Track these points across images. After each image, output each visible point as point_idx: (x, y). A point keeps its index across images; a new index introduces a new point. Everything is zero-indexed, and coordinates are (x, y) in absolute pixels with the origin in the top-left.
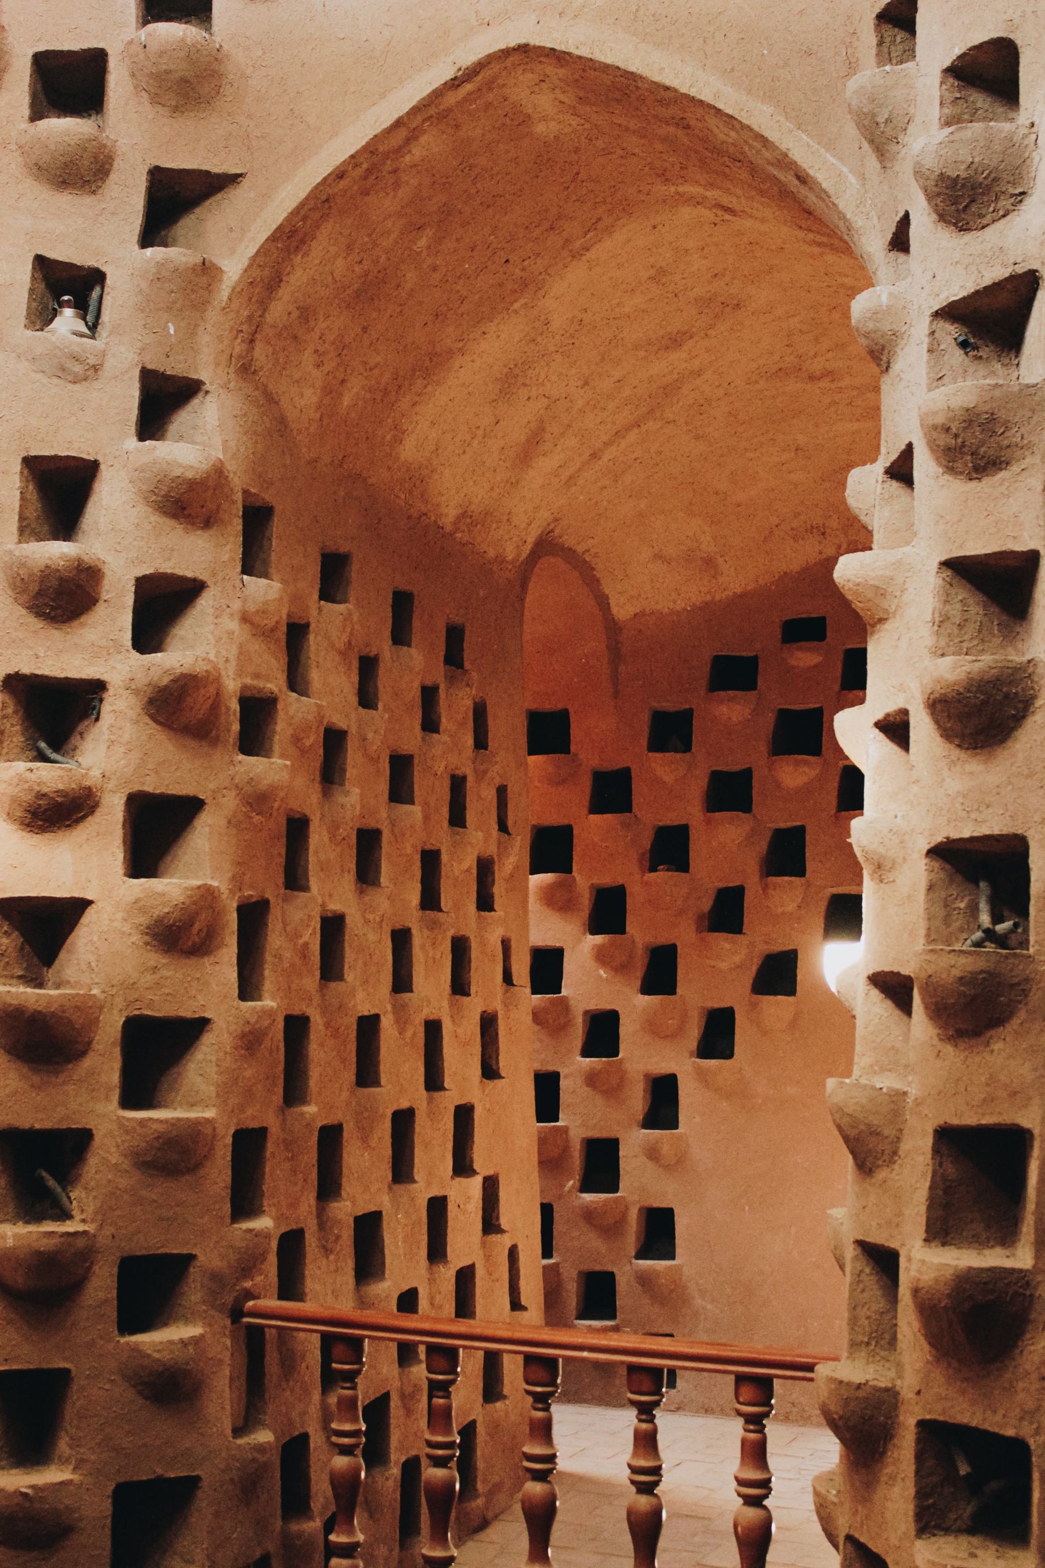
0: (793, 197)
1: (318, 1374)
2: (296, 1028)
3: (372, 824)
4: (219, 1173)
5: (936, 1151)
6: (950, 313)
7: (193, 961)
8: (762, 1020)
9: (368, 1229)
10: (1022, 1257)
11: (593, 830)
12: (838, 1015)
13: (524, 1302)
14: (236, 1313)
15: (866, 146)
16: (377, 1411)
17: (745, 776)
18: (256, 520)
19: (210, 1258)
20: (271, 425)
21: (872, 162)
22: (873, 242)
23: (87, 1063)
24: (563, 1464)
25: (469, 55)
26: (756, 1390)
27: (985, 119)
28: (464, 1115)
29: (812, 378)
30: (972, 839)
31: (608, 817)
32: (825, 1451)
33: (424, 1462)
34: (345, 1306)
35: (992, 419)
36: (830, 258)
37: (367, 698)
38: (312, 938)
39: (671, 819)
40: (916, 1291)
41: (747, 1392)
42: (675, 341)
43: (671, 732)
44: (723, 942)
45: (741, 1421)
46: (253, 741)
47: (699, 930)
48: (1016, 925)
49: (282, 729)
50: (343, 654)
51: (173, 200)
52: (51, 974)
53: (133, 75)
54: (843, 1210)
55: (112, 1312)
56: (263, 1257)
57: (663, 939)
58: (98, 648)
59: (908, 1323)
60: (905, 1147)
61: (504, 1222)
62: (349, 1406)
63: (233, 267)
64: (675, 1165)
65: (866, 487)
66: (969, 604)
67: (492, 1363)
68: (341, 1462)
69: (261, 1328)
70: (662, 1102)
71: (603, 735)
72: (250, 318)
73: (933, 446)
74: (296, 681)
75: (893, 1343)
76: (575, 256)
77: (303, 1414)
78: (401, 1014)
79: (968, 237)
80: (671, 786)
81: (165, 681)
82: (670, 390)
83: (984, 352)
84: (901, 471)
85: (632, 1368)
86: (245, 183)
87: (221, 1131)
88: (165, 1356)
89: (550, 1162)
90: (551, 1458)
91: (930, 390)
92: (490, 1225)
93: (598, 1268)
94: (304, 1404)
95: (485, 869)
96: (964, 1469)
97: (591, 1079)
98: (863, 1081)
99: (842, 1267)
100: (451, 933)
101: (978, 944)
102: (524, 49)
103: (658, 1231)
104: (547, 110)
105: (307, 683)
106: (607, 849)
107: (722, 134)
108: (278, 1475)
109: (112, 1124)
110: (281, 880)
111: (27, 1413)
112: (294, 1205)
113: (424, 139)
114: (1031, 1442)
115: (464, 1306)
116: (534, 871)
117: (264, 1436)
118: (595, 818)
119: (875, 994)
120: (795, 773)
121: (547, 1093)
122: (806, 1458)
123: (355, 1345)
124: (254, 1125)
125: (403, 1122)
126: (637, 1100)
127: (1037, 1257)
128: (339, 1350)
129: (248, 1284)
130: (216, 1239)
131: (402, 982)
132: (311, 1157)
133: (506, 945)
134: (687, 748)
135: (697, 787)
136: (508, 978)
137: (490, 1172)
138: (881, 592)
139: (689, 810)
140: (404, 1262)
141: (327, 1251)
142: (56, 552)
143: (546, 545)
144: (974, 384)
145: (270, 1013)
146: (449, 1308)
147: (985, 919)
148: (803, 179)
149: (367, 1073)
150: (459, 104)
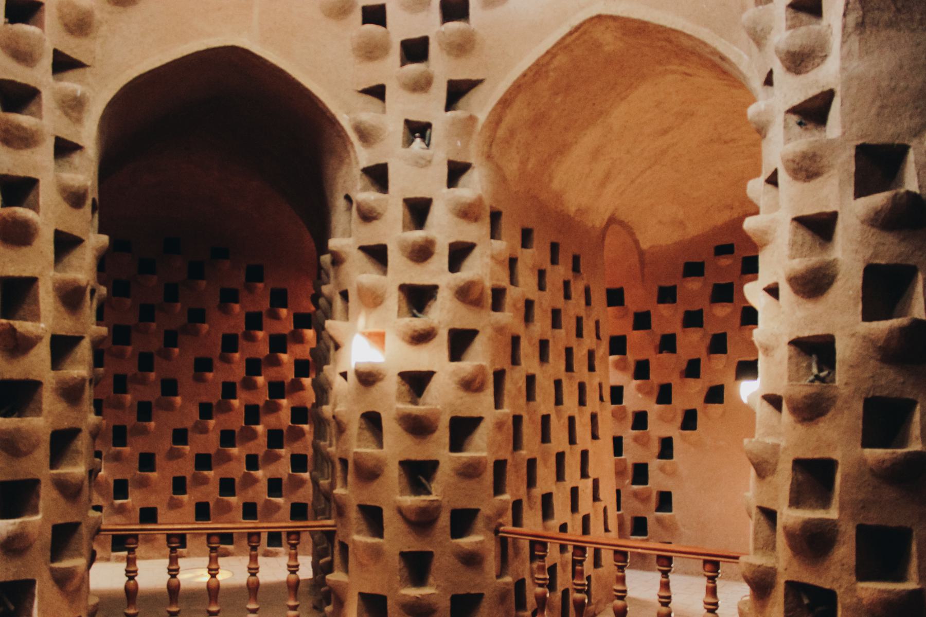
0: (720, 68)
1: (528, 555)
2: (517, 420)
3: (545, 337)
4: (489, 477)
5: (794, 469)
6: (793, 111)
7: (476, 394)
8: (709, 415)
9: (547, 499)
10: (833, 514)
11: (635, 337)
12: (749, 412)
13: (610, 528)
14: (496, 532)
15: (751, 42)
16: (552, 570)
17: (700, 313)
18: (495, 217)
19: (486, 510)
20: (500, 178)
21: (754, 48)
22: (756, 82)
23: (436, 435)
24: (630, 594)
25: (576, 21)
26: (712, 566)
27: (806, 24)
28: (585, 454)
29: (726, 142)
30: (809, 337)
31: (642, 331)
32: (744, 591)
33: (571, 591)
34: (539, 530)
35: (814, 155)
36: (733, 91)
37: (541, 287)
38: (522, 384)
39: (669, 331)
40: (785, 528)
41: (708, 567)
42: (665, 132)
43: (667, 295)
44: (691, 382)
45: (705, 579)
46: (497, 306)
47: (681, 377)
48: (829, 373)
49: (508, 300)
50: (532, 269)
51: (457, 92)
52: (421, 400)
53: (440, 45)
54: (750, 492)
55: (448, 530)
56: (507, 509)
57: (666, 381)
58: (435, 272)
59: (781, 540)
60: (780, 467)
61: (601, 497)
62: (541, 569)
63: (482, 116)
64: (673, 474)
65: (756, 188)
66: (805, 235)
67: (597, 553)
68: (539, 590)
69: (506, 538)
70: (666, 448)
71: (636, 299)
72: (490, 137)
73: (787, 169)
74: (513, 281)
75: (774, 548)
76: (622, 99)
77: (523, 571)
78: (558, 413)
79: (801, 77)
80: (667, 318)
81: (462, 284)
82: (664, 152)
83: (809, 126)
84: (773, 180)
85: (659, 557)
86: (485, 83)
87: (489, 461)
88: (470, 548)
89: (620, 473)
90: (625, 591)
91: (785, 144)
92: (596, 498)
93: (639, 515)
94: (523, 567)
95: (591, 354)
96: (806, 601)
97: (636, 439)
98: (760, 440)
99: (750, 517)
100: (578, 381)
101: (812, 381)
102: (599, 17)
103: (665, 501)
104: (609, 40)
105: (517, 281)
106: (640, 344)
107: (686, 43)
108: (513, 594)
109: (447, 459)
110: (509, 361)
111: (13, 498)
112: (518, 490)
113: (558, 58)
114: (838, 592)
115: (586, 530)
116: (611, 354)
117: (508, 579)
118: (635, 332)
119: (765, 403)
120: (722, 311)
121: (618, 444)
122: (734, 594)
123: (544, 545)
124: (501, 458)
125: (560, 457)
126: (655, 448)
127: (840, 513)
128: (538, 547)
129: (501, 521)
130: (489, 504)
131: (559, 401)
132: (524, 471)
133: (600, 385)
134: (674, 301)
135: (679, 317)
136: (601, 399)
137: (596, 477)
138: (765, 233)
139: (675, 327)
140: (561, 511)
141: (531, 508)
142: (417, 235)
143: (612, 220)
144: (804, 141)
145: (506, 414)
146: (580, 531)
147: (815, 370)
148: (723, 58)
149: (545, 438)
150: (574, 41)
